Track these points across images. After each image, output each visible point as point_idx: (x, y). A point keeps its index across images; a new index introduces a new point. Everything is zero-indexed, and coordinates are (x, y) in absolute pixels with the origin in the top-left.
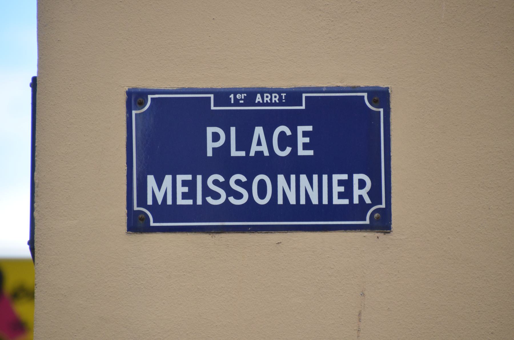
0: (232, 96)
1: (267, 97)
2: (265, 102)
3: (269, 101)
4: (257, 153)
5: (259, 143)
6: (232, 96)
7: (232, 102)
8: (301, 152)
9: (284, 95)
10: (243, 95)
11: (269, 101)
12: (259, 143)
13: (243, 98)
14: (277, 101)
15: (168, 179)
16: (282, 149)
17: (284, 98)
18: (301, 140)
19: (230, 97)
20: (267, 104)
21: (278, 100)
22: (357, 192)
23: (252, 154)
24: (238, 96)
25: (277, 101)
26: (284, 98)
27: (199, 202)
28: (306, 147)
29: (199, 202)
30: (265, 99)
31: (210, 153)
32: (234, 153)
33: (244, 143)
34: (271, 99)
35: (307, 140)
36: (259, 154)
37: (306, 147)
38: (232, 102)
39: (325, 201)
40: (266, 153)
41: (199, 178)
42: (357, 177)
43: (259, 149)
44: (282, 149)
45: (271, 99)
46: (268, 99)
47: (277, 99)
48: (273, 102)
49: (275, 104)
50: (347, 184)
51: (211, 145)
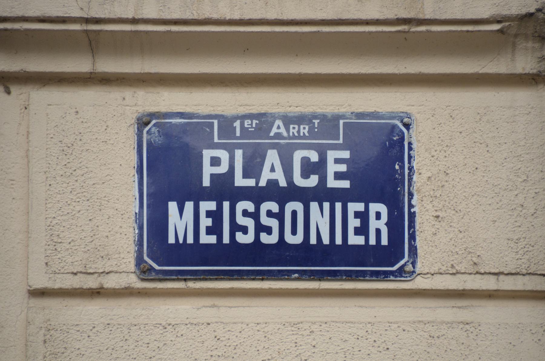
0: (237, 124)
1: (294, 128)
2: (291, 134)
3: (296, 134)
4: (269, 182)
5: (273, 170)
6: (237, 124)
7: (238, 134)
8: (332, 183)
9: (316, 122)
10: (255, 122)
11: (296, 134)
12: (273, 170)
13: (254, 125)
14: (307, 134)
15: (189, 206)
16: (305, 175)
17: (316, 126)
18: (332, 168)
19: (235, 125)
20: (294, 137)
21: (308, 132)
22: (373, 224)
23: (263, 183)
24: (247, 123)
25: (307, 134)
26: (316, 126)
27: (226, 240)
28: (338, 176)
29: (226, 240)
30: (291, 130)
31: (206, 182)
32: (240, 181)
33: (252, 168)
34: (299, 132)
35: (343, 168)
36: (273, 183)
37: (338, 176)
38: (238, 134)
39: (339, 241)
40: (283, 183)
41: (226, 205)
42: (374, 207)
43: (273, 176)
44: (305, 175)
45: (299, 132)
46: (295, 131)
47: (306, 131)
48: (302, 134)
49: (304, 137)
50: (363, 216)
51: (208, 171)
